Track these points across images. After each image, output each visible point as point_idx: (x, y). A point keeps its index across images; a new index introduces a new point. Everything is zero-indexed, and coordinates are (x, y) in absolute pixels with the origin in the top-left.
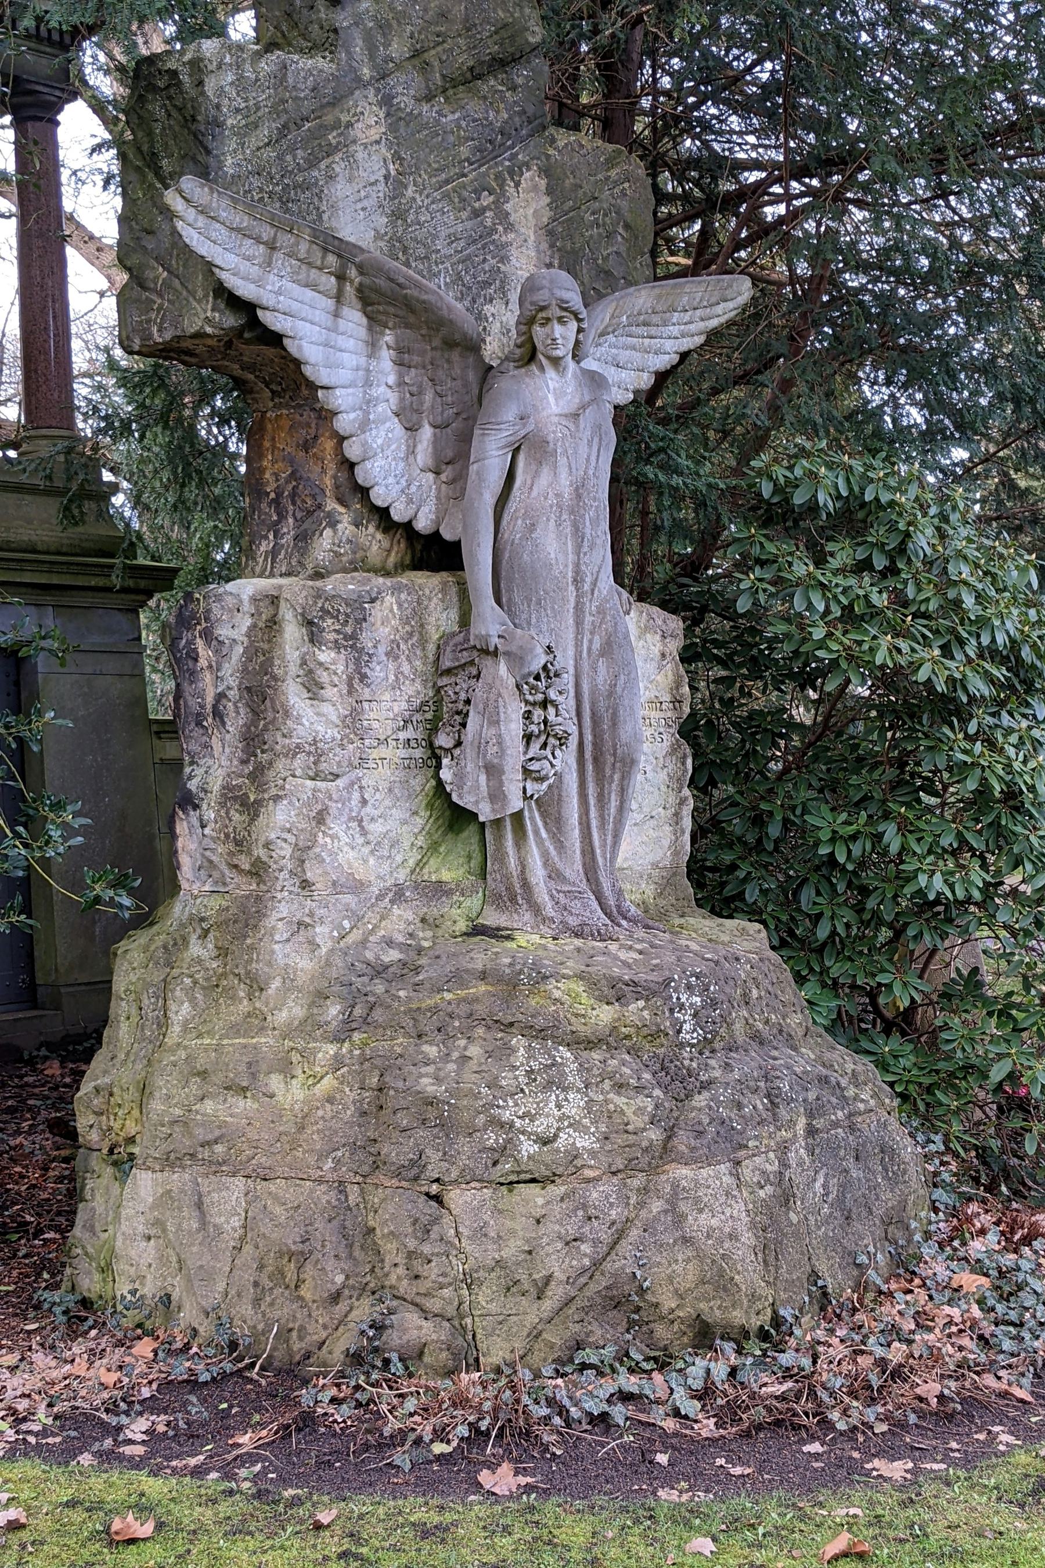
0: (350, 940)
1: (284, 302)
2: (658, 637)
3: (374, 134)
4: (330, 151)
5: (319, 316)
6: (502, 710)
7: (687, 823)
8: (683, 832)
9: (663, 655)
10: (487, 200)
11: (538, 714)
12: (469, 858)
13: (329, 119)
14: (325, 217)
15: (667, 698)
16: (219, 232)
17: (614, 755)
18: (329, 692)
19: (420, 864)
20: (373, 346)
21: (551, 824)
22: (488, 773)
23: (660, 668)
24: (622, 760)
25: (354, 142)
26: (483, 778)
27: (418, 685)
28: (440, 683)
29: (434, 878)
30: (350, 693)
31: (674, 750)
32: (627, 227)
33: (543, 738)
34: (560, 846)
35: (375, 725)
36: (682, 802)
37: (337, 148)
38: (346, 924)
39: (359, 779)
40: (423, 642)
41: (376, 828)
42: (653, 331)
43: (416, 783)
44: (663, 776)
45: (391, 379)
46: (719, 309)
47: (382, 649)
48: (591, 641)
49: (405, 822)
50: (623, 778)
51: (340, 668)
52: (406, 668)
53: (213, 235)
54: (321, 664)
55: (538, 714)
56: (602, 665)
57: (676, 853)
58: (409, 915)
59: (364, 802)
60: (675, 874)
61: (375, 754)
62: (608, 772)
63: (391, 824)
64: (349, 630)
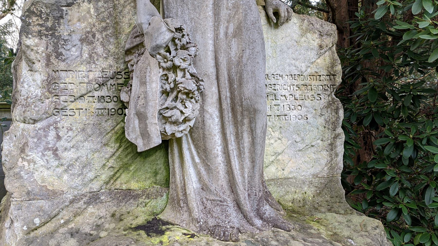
0: (40, 232)
2: (316, 35)
6: (148, 74)
7: (340, 150)
8: (337, 155)
9: (321, 47)
11: (172, 76)
12: (156, 174)
15: (324, 72)
17: (242, 106)
18: (38, 66)
19: (113, 178)
21: (201, 154)
22: (139, 118)
23: (319, 55)
24: (248, 110)
26: (137, 122)
27: (111, 61)
28: (127, 60)
29: (124, 187)
30: (47, 65)
31: (329, 105)
33: (175, 93)
34: (208, 169)
35: (70, 87)
36: (336, 137)
38: (37, 221)
39: (56, 123)
40: (117, 34)
41: (69, 156)
43: (108, 125)
44: (321, 120)
47: (76, 38)
48: (227, 28)
49: (97, 151)
50: (250, 122)
51: (41, 49)
52: (100, 50)
54: (28, 47)
55: (172, 76)
56: (234, 44)
57: (332, 168)
58: (103, 212)
59: (59, 138)
60: (331, 181)
62: (239, 118)
63: (83, 152)
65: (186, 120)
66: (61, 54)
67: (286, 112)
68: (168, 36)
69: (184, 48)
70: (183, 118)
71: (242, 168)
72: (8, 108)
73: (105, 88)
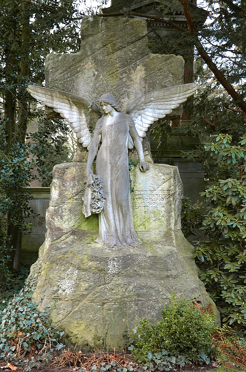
1: (58, 106)
3: (91, 66)
4: (78, 72)
5: (67, 108)
10: (124, 75)
13: (78, 65)
14: (75, 86)
16: (41, 95)
20: (80, 114)
25: (85, 69)
32: (172, 74)
37: (79, 71)
42: (168, 100)
45: (85, 120)
46: (189, 92)
47: (68, 179)
53: (39, 95)
61: (67, 201)
64: (61, 175)
65: (98, 208)
66: (64, 185)
67: (148, 205)
68: (93, 181)
69: (98, 185)
70: (97, 207)
71: (120, 225)
72: (48, 191)
73: (78, 196)
